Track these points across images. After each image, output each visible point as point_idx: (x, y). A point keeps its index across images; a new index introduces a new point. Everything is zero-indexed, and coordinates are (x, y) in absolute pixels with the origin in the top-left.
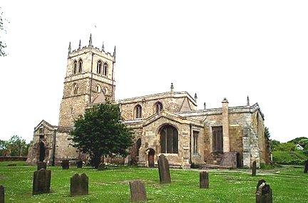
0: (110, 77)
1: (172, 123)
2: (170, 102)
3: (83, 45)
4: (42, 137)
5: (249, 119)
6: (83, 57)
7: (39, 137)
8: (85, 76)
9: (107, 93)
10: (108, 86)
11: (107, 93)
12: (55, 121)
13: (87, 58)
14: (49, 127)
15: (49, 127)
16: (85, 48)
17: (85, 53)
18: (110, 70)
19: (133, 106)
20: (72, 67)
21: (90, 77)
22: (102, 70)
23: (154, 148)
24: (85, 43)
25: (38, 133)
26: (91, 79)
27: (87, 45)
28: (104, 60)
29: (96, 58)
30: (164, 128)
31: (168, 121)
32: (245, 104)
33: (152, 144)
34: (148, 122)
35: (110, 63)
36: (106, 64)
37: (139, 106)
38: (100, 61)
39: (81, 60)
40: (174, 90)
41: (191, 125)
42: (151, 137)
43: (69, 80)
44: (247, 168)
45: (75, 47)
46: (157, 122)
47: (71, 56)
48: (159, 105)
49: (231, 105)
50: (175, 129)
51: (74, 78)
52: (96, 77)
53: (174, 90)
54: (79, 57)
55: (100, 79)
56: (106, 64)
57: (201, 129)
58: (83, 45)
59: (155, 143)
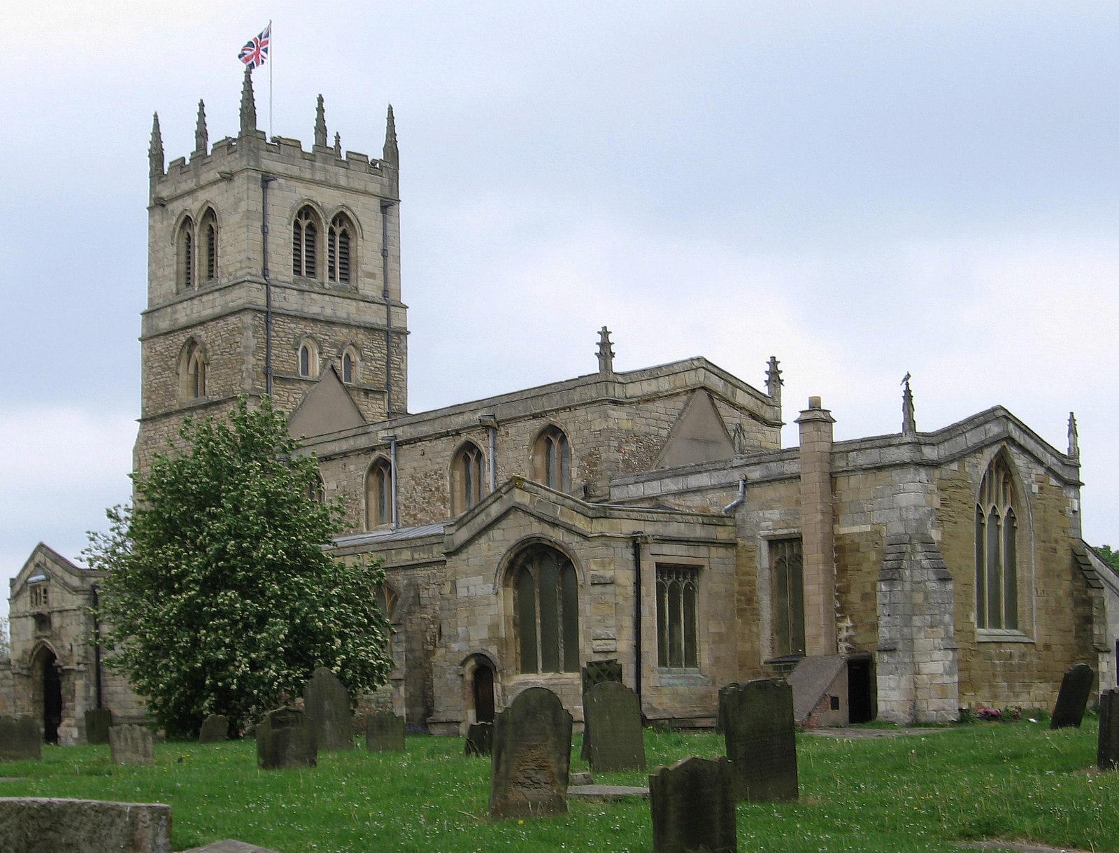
0: (370, 288)
1: (558, 536)
2: (598, 425)
3: (214, 137)
4: (42, 621)
5: (413, 698)
6: (218, 197)
7: (31, 623)
8: (238, 298)
9: (360, 374)
10: (361, 337)
11: (360, 374)
12: (75, 552)
13: (235, 203)
14: (67, 577)
15: (67, 577)
16: (180, 164)
17: (228, 177)
18: (366, 251)
19: (447, 448)
20: (171, 253)
21: (261, 302)
22: (323, 255)
23: (493, 651)
24: (225, 125)
25: (25, 604)
26: (268, 314)
27: (234, 129)
28: (329, 201)
29: (285, 200)
30: (530, 560)
31: (537, 529)
32: (894, 426)
33: (485, 634)
34: (463, 535)
35: (365, 212)
36: (341, 218)
37: (470, 447)
38: (307, 211)
39: (210, 214)
40: (619, 365)
41: (637, 544)
42: (479, 605)
43: (164, 325)
44: (890, 724)
45: (179, 146)
46: (496, 533)
47: (165, 192)
48: (551, 436)
49: (841, 433)
50: (565, 563)
51: (183, 314)
52: (290, 301)
53: (619, 365)
54: (203, 196)
55: (318, 305)
56: (341, 218)
57: (716, 552)
58: (214, 137)
59: (494, 627)
